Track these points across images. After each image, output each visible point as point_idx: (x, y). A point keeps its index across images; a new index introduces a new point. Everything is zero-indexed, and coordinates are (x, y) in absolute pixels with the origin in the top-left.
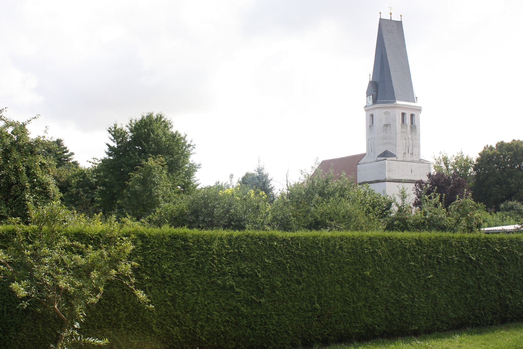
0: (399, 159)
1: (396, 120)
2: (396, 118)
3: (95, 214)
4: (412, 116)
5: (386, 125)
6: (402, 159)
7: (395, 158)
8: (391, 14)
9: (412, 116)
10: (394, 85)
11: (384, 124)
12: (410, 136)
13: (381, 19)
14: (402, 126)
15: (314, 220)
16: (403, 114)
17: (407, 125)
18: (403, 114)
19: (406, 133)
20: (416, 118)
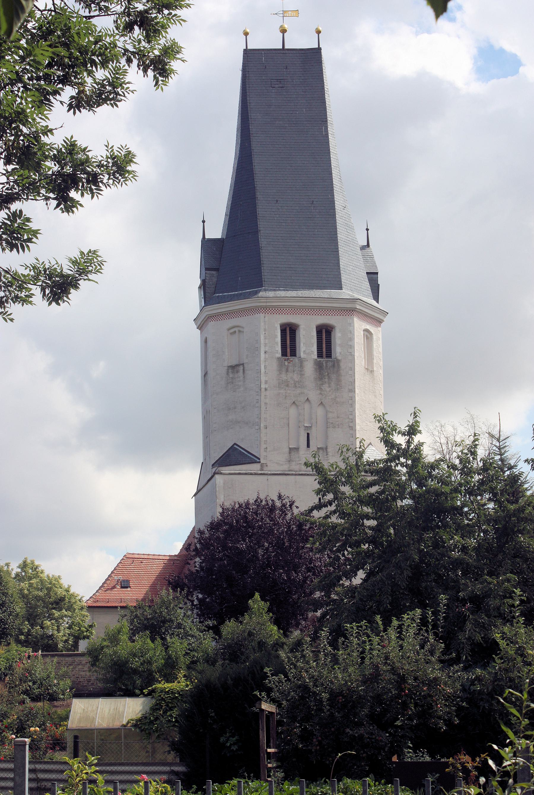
0: (272, 468)
1: (258, 349)
2: (258, 341)
3: (283, 706)
4: (325, 334)
5: (234, 368)
6: (285, 468)
7: (254, 468)
8: (318, 32)
9: (325, 334)
10: (263, 242)
11: (226, 364)
12: (313, 395)
13: (247, 53)
14: (281, 365)
15: (214, 659)
16: (289, 333)
17: (301, 361)
18: (289, 333)
19: (298, 385)
20: (337, 337)
